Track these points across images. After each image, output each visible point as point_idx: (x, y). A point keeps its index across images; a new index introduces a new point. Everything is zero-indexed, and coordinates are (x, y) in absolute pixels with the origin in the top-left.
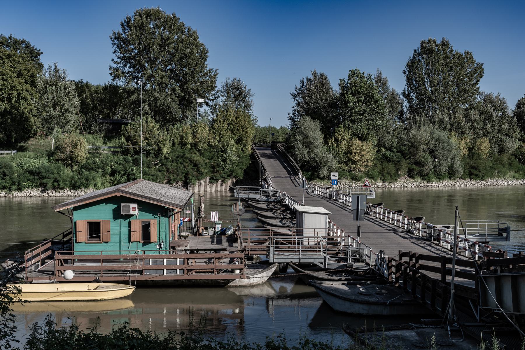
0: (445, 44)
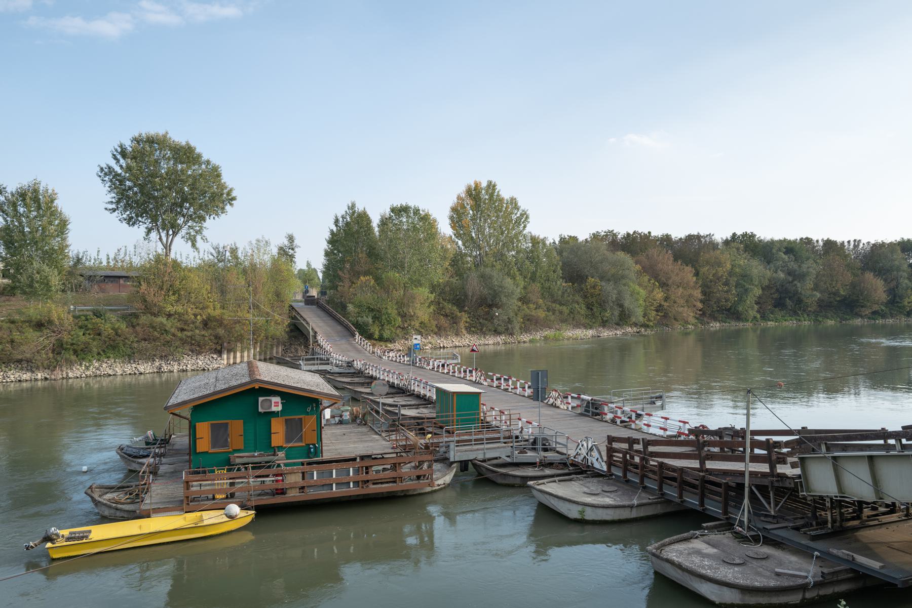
0: (491, 186)
